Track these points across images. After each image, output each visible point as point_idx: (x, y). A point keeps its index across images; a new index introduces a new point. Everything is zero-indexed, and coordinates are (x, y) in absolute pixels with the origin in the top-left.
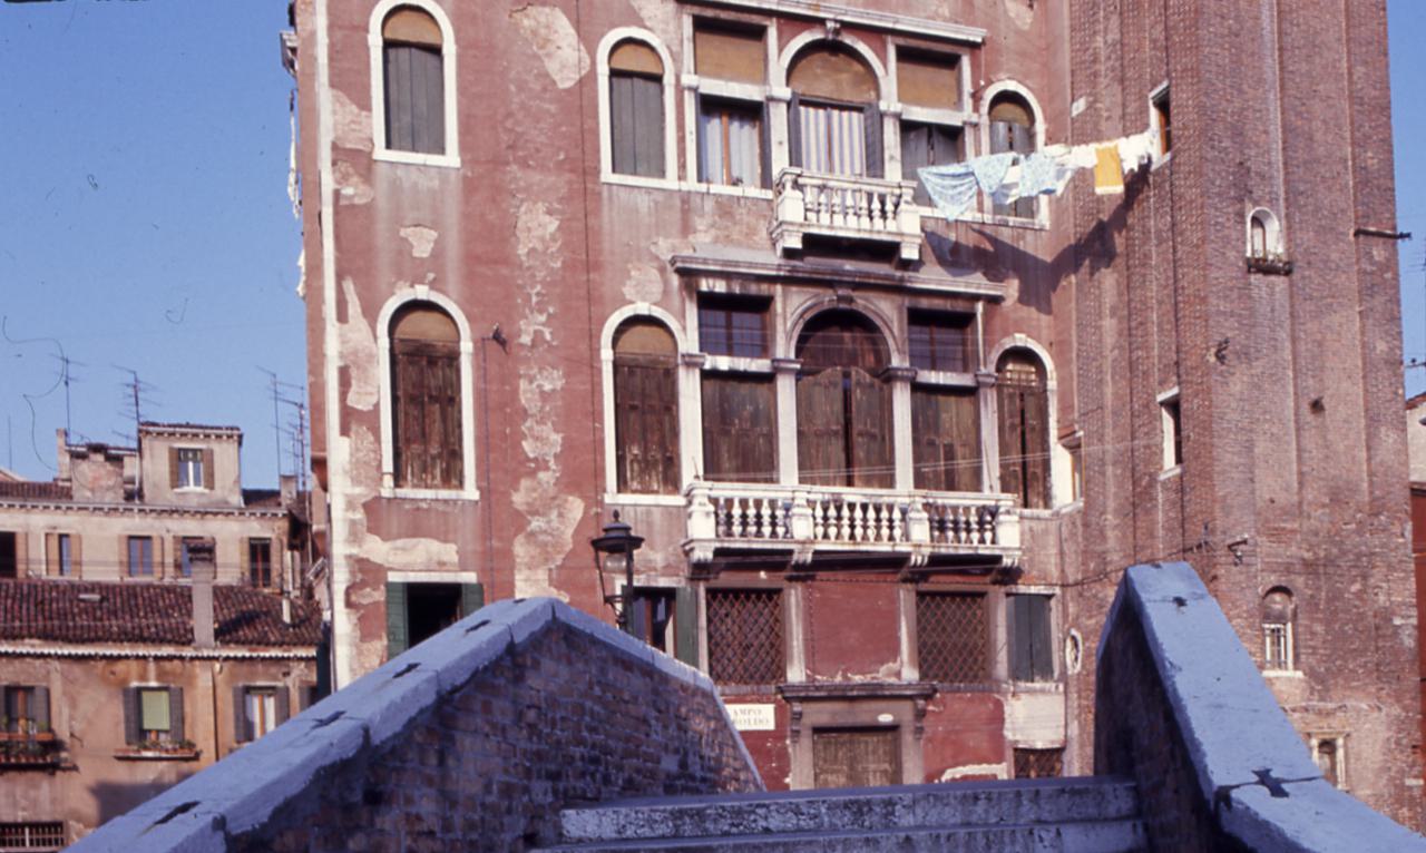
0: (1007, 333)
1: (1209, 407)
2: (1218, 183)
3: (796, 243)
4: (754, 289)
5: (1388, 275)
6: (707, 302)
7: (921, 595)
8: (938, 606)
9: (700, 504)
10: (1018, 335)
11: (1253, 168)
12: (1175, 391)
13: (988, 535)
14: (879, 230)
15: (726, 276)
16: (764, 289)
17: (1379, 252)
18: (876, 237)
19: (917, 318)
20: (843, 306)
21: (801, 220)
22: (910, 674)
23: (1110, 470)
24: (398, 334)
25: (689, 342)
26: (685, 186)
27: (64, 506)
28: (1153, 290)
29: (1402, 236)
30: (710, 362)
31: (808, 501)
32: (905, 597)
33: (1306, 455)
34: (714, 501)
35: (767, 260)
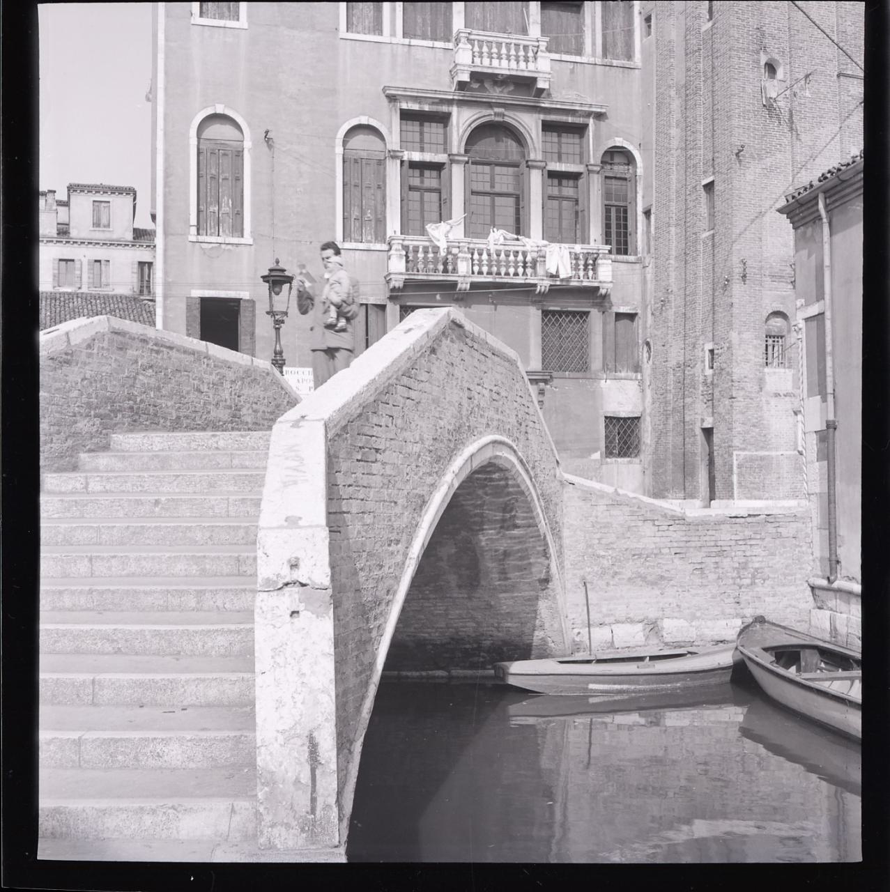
0: (609, 137)
1: (731, 189)
2: (741, 41)
6: (406, 115)
7: (545, 313)
8: (557, 320)
9: (396, 250)
10: (617, 139)
11: (767, 31)
13: (591, 273)
15: (416, 99)
16: (445, 109)
18: (514, 73)
19: (547, 127)
20: (498, 119)
21: (470, 63)
23: (673, 229)
24: (205, 135)
25: (393, 141)
26: (394, 40)
27: (145, 245)
28: (700, 111)
30: (406, 156)
31: (402, 245)
32: (533, 315)
34: (406, 248)
35: (447, 88)
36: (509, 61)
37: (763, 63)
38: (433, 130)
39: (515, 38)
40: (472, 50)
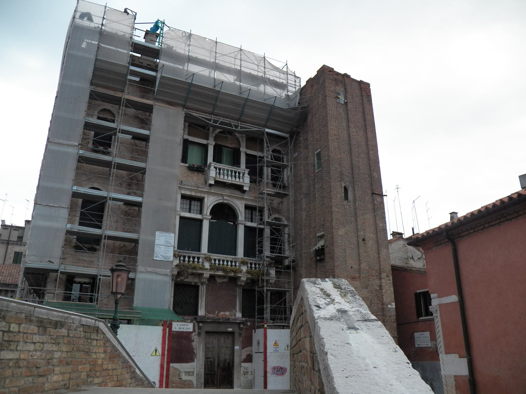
3: (212, 182)
4: (199, 195)
5: (382, 206)
12: (323, 233)
14: (237, 181)
16: (202, 195)
17: (379, 199)
18: (234, 183)
19: (247, 207)
22: (239, 315)
29: (385, 196)
33: (361, 254)
36: (239, 179)
37: (343, 185)
38: (195, 205)
39: (235, 169)
40: (216, 171)
